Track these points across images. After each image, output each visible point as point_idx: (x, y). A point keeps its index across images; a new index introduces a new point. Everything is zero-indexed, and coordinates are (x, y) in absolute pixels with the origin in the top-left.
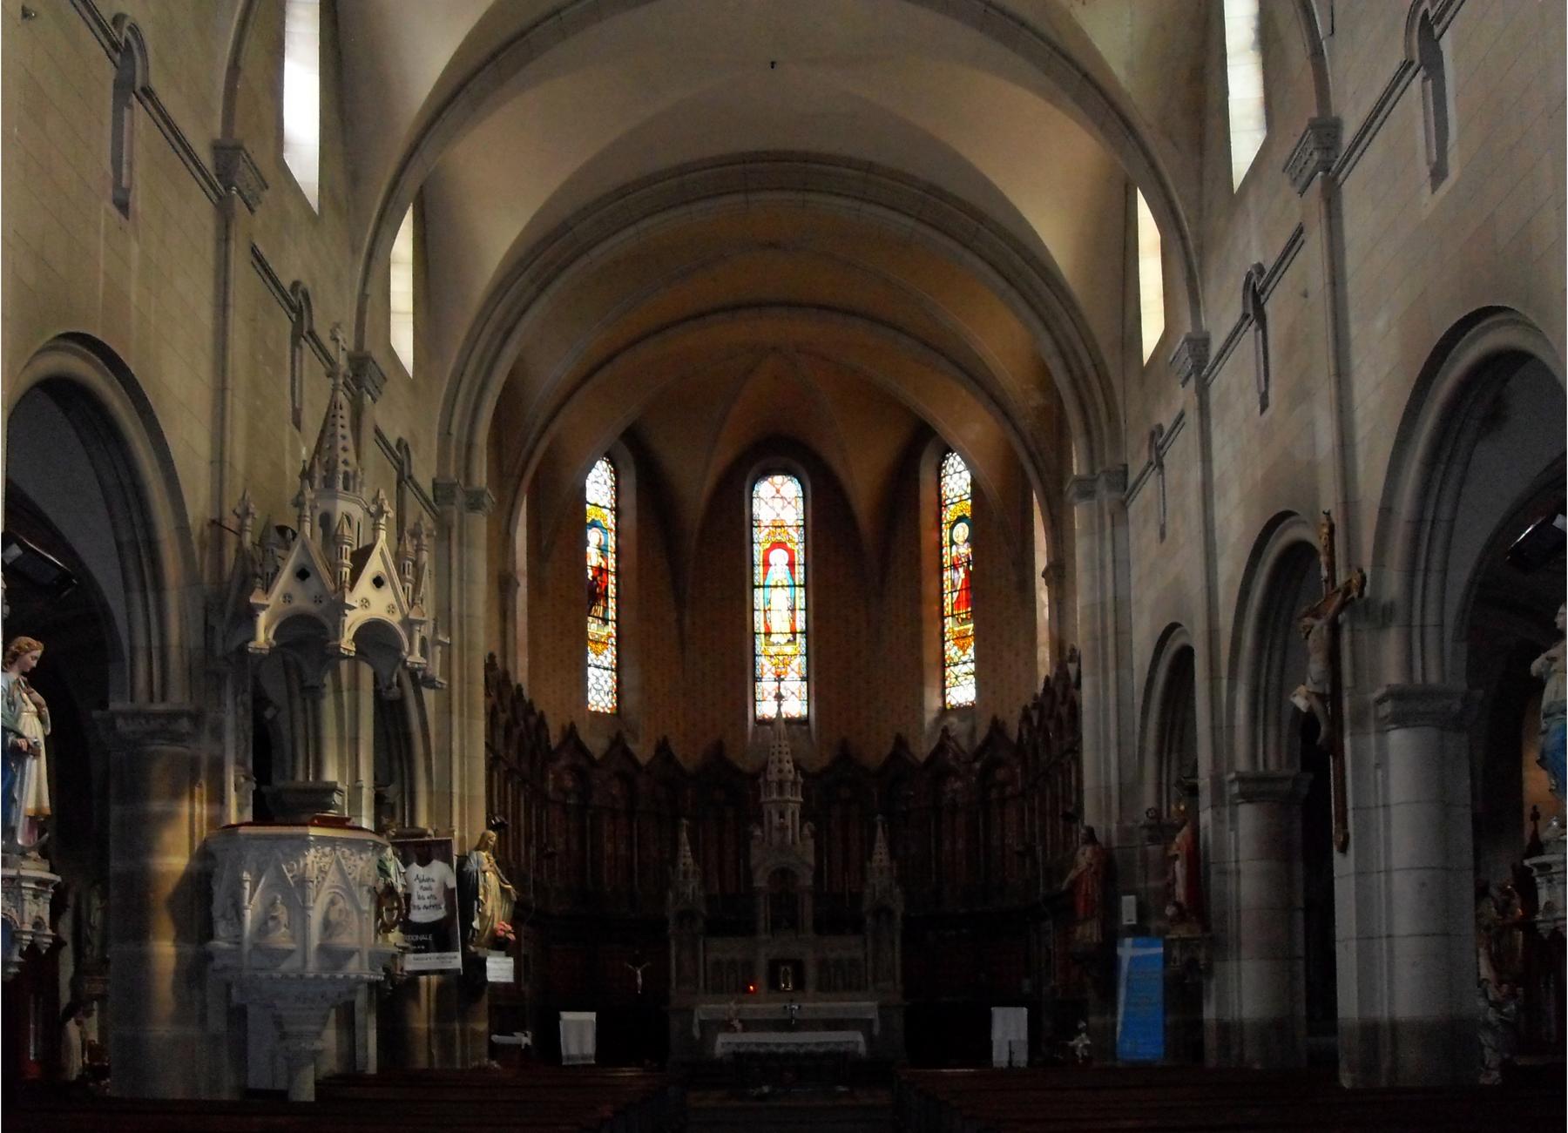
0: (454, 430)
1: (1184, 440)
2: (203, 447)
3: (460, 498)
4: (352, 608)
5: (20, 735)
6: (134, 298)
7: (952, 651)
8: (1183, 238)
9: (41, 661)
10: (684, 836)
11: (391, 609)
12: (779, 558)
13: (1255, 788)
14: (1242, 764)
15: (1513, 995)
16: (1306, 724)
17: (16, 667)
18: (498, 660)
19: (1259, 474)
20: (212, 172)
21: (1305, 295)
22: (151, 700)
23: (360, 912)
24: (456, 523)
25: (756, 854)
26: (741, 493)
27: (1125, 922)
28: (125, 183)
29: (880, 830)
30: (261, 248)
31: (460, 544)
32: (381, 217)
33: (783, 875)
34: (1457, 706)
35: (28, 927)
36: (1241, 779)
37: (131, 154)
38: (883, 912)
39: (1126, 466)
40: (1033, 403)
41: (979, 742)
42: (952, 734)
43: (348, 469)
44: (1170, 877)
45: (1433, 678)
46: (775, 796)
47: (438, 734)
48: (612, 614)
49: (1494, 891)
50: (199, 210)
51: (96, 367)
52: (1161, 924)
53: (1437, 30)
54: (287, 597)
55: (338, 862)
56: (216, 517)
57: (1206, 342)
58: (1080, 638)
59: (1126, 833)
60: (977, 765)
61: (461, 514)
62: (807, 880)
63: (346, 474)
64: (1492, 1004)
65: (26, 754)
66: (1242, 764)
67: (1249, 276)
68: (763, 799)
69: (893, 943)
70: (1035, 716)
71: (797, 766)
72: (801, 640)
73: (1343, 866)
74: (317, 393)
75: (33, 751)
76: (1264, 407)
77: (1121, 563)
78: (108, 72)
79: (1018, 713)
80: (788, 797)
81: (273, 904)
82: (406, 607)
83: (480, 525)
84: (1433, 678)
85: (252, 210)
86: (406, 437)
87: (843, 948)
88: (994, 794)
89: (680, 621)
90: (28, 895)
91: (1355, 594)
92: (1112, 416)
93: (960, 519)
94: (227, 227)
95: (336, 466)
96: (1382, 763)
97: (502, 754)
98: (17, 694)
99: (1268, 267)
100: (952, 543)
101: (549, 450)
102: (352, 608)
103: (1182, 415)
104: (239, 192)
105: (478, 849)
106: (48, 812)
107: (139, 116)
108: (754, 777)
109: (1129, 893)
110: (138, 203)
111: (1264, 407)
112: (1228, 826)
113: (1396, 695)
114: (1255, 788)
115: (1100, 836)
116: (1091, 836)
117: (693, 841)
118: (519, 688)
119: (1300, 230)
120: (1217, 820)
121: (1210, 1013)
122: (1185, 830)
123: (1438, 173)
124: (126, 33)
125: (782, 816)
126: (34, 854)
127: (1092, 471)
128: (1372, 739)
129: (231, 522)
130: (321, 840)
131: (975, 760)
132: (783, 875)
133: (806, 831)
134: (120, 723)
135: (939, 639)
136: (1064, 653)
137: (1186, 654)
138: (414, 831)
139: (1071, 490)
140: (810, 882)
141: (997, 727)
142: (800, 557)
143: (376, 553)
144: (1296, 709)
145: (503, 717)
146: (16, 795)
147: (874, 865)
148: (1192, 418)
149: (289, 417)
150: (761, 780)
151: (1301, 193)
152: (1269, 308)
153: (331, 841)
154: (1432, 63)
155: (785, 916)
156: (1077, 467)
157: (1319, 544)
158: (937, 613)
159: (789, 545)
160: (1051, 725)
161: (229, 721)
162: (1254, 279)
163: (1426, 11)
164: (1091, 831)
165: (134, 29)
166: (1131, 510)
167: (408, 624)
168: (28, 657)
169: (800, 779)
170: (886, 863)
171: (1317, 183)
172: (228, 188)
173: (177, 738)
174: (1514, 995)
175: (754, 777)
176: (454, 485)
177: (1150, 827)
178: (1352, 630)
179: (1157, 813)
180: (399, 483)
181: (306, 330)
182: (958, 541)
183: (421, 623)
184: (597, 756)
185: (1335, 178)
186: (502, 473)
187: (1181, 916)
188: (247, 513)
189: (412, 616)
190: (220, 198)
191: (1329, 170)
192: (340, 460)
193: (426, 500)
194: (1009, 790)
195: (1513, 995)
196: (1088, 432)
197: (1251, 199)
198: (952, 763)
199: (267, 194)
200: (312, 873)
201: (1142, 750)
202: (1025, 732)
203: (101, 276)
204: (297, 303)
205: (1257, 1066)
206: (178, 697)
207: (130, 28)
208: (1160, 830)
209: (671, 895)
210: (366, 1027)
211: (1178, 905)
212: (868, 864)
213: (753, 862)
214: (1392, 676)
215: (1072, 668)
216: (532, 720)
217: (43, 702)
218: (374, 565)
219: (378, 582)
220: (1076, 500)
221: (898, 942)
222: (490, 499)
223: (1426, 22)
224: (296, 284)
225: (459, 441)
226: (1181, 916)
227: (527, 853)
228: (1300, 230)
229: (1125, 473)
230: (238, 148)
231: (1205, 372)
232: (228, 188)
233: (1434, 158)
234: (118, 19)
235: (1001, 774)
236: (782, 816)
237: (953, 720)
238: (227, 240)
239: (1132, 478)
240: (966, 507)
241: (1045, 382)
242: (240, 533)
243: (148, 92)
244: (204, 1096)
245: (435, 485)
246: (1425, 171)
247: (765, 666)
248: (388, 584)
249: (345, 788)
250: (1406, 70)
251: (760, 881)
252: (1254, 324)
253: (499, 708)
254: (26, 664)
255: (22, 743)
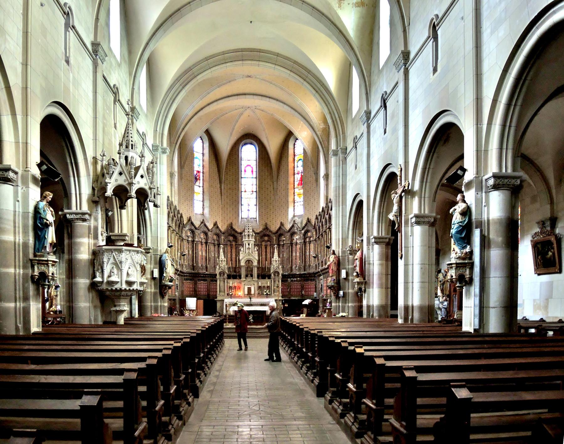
0: (158, 130)
1: (363, 143)
2: (91, 136)
3: (160, 150)
4: (135, 184)
5: (47, 220)
6: (71, 91)
7: (297, 198)
8: (365, 82)
9: (52, 199)
10: (221, 251)
11: (146, 184)
12: (249, 169)
13: (378, 241)
14: (375, 234)
15: (446, 300)
16: (393, 223)
17: (45, 200)
18: (170, 198)
19: (383, 152)
20: (91, 51)
21: (398, 102)
22: (77, 209)
23: (137, 271)
24: (159, 157)
25: (241, 256)
26: (238, 150)
27: (343, 277)
28: (68, 55)
29: (276, 249)
30: (105, 75)
31: (160, 164)
32: (138, 65)
33: (249, 261)
34: (433, 220)
35: (50, 274)
36: (375, 238)
37: (69, 47)
38: (276, 273)
39: (347, 147)
40: (321, 127)
41: (303, 225)
42: (296, 222)
43: (133, 143)
44: (355, 265)
45: (427, 212)
46: (247, 239)
47: (154, 219)
48: (201, 185)
49: (442, 271)
50: (89, 62)
51: (61, 110)
52: (352, 278)
53: (437, 28)
54: (116, 180)
55: (131, 257)
56: (95, 156)
57: (370, 113)
58: (332, 196)
59: (343, 252)
60: (303, 232)
61: (160, 155)
62: (255, 263)
63: (132, 145)
64: (441, 303)
65: (49, 226)
66: (375, 234)
67: (383, 95)
68: (243, 240)
69: (279, 281)
70: (319, 218)
71: (253, 231)
72: (255, 193)
73: (401, 263)
74: (122, 121)
75: (51, 224)
76: (385, 132)
77: (344, 175)
78: (63, 21)
79: (315, 217)
80: (250, 239)
81: (113, 268)
82: (150, 184)
83: (165, 158)
84: (427, 212)
85: (103, 63)
86: (145, 132)
87: (266, 282)
88: (308, 240)
89: (221, 187)
90: (50, 265)
91: (406, 188)
92: (344, 133)
93: (300, 160)
94: (96, 68)
95: (129, 142)
96: (412, 235)
97: (171, 225)
98: (46, 208)
99: (388, 93)
100: (297, 167)
101: (184, 136)
102: (135, 184)
103: (363, 134)
104: (99, 58)
105: (165, 253)
106: (55, 242)
107: (71, 34)
108: (241, 233)
109: (344, 269)
110: (72, 60)
111: (385, 132)
112: (371, 251)
113: (416, 216)
114: (378, 241)
115: (336, 253)
116: (334, 253)
117: (224, 252)
118: (176, 206)
119: (397, 83)
120: (368, 249)
121: (365, 303)
122: (360, 252)
123: (435, 70)
124: (68, 9)
125: (249, 245)
126: (52, 254)
127: (337, 148)
128: (410, 228)
129: (99, 157)
130: (126, 250)
131: (302, 230)
132: (249, 261)
133: (255, 249)
134: (68, 216)
135: (293, 195)
136: (328, 201)
137: (361, 202)
138: (147, 248)
139: (331, 153)
140: (256, 264)
141: (309, 221)
142: (255, 170)
143: (141, 168)
144: (390, 220)
145: (171, 215)
146: (46, 237)
147: (274, 259)
148: (365, 135)
149: (113, 126)
150: (243, 234)
151: (398, 72)
152: (388, 104)
153: (130, 251)
154: (435, 37)
155: (249, 274)
156: (333, 146)
157: (398, 173)
158: (293, 188)
159: (251, 166)
160: (324, 220)
161: (100, 216)
162: (384, 95)
163: (434, 22)
164: (334, 251)
165: (70, 8)
166: (348, 160)
167: (150, 189)
168: (48, 198)
169: (254, 234)
170: (277, 259)
171: (402, 70)
172: (96, 57)
173: (84, 220)
174: (447, 301)
175: (241, 233)
176: (158, 146)
177: (350, 251)
178: (405, 198)
179: (352, 247)
180: (143, 145)
181: (117, 99)
182: (299, 167)
183: (154, 188)
184: (197, 227)
185: (408, 68)
186: (171, 143)
187: (358, 276)
188: (104, 155)
189: (151, 187)
190: (94, 59)
191: (406, 66)
192: (130, 140)
193: (150, 150)
194: (311, 239)
195: (446, 300)
196: (337, 137)
197: (384, 72)
198: (296, 231)
199: (106, 58)
200: (123, 260)
201: (348, 228)
202: (316, 222)
203: (62, 84)
204: (115, 91)
205: (377, 318)
206: (85, 208)
207: (69, 7)
208: (353, 252)
209: (218, 267)
210: (135, 304)
211: (357, 273)
212: (272, 259)
213: (241, 258)
214: (416, 211)
215: (330, 205)
216: (179, 216)
217: (53, 210)
218: (141, 172)
219: (142, 177)
220: (332, 156)
221: (280, 281)
222: (168, 151)
223: (434, 27)
224: (114, 85)
225: (159, 133)
226: (358, 276)
227: (177, 254)
228: (397, 83)
229: (346, 149)
230: (99, 44)
231: (369, 122)
232: (96, 57)
233: (434, 65)
234: (65, 4)
235: (309, 234)
236: (249, 245)
237: (296, 218)
238: (96, 72)
239: (348, 152)
240: (302, 157)
241: (325, 121)
242: (102, 161)
243: (74, 27)
244: (93, 323)
245: (153, 146)
246: (432, 69)
247: (244, 201)
248: (145, 177)
249: (129, 235)
250: (428, 38)
251: (243, 263)
252: (384, 109)
253: (170, 212)
254: (48, 199)
255: (48, 222)
